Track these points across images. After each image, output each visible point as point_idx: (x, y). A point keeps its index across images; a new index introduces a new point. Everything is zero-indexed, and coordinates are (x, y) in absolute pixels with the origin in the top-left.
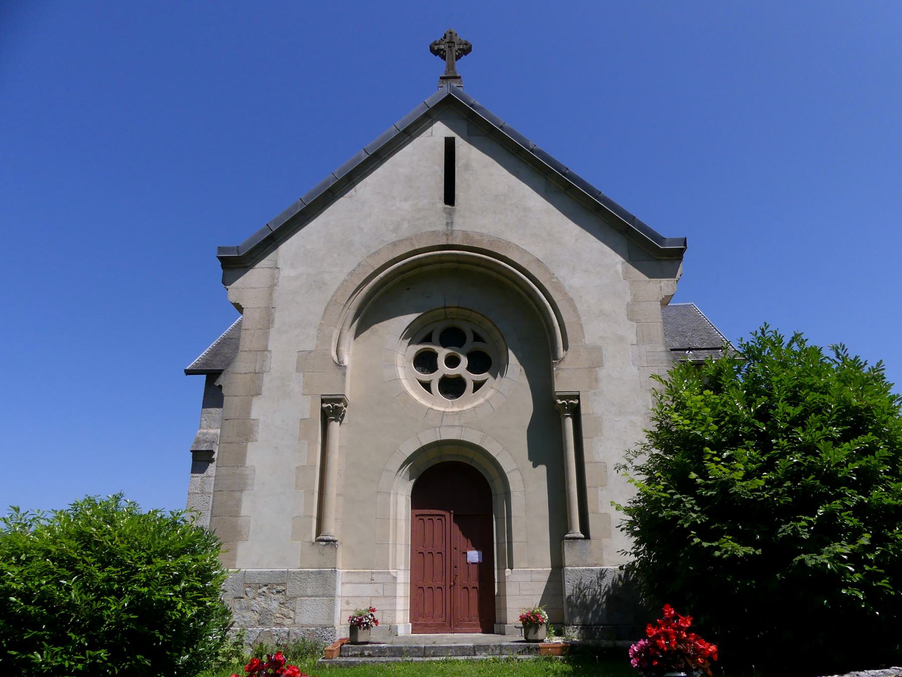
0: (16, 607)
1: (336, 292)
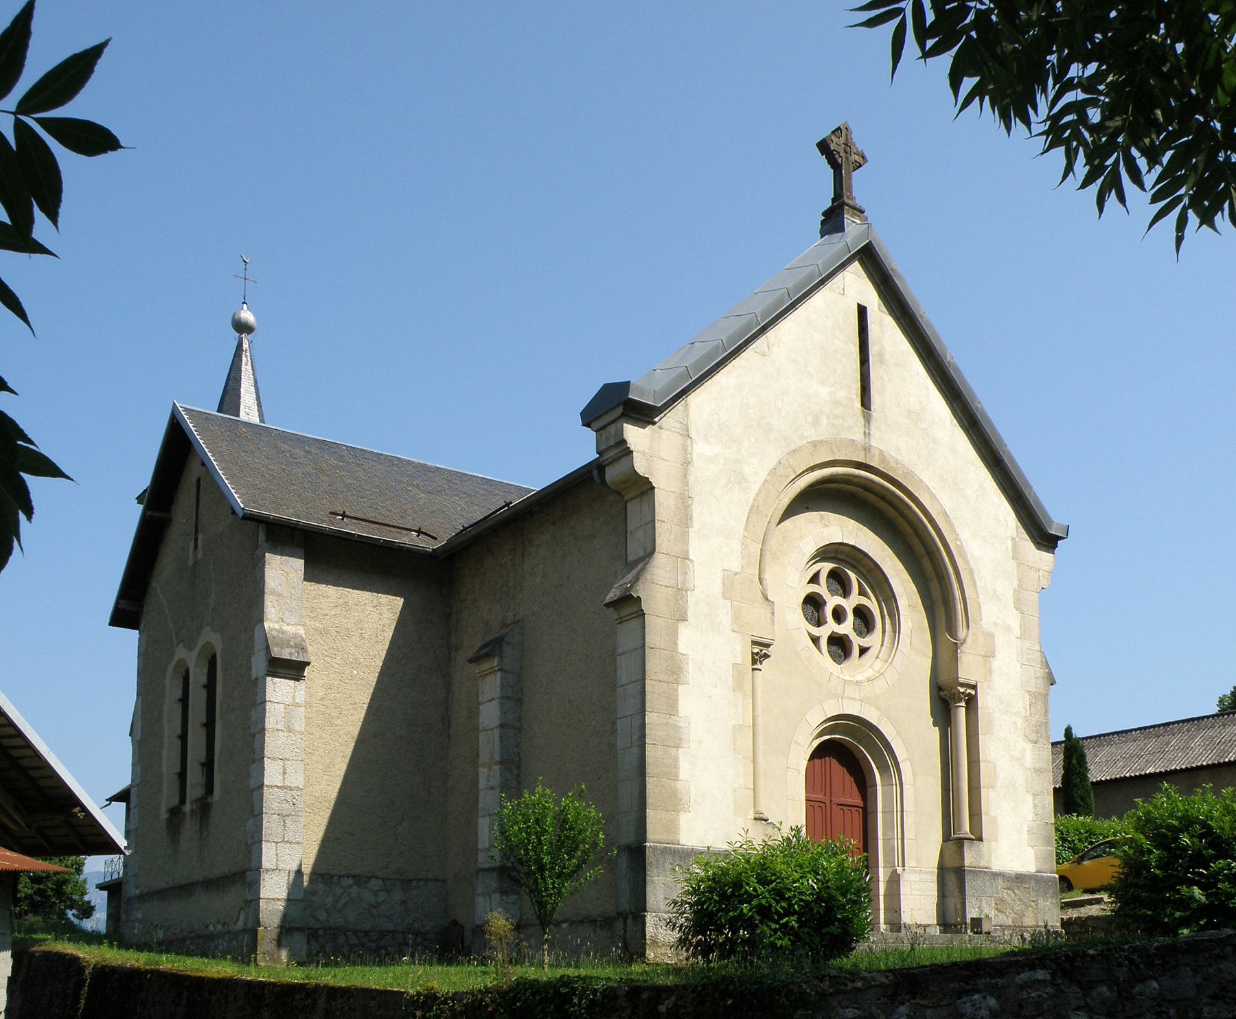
1: (757, 495)
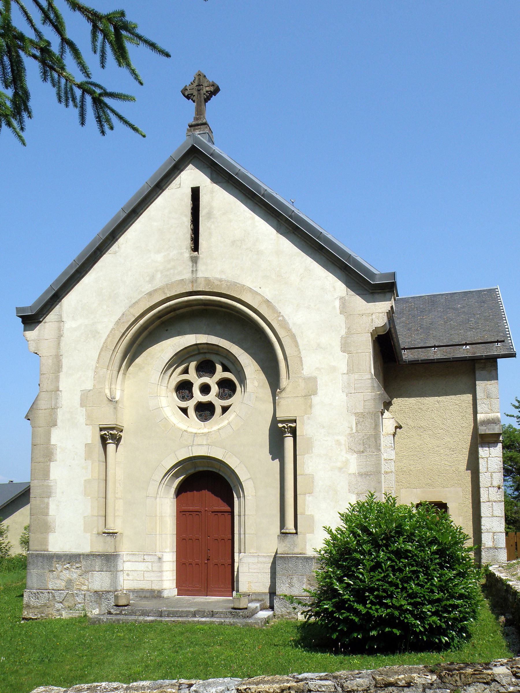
1: (106, 339)
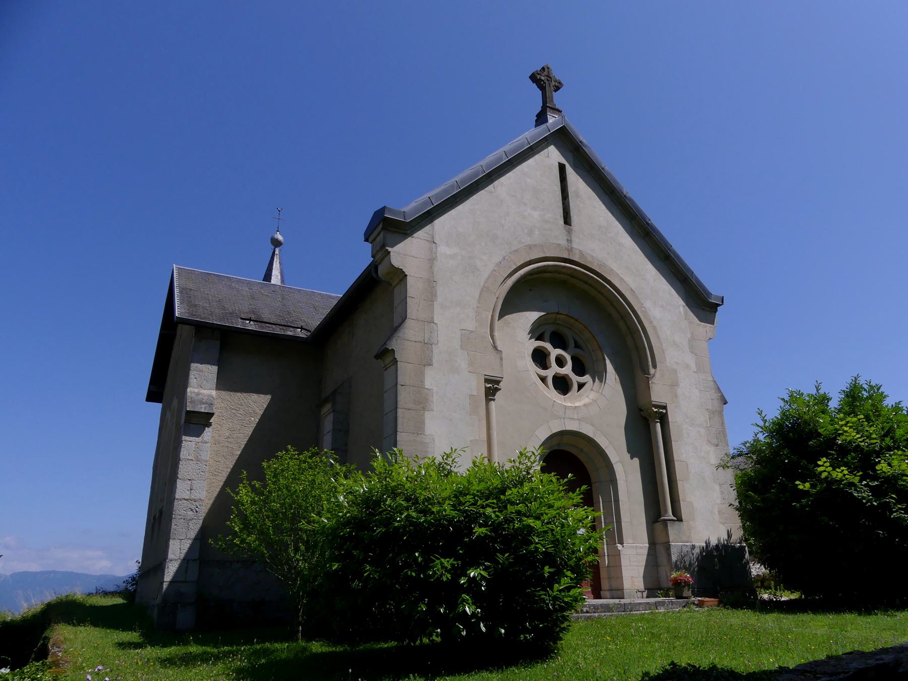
0: (564, 548)
1: (487, 279)
